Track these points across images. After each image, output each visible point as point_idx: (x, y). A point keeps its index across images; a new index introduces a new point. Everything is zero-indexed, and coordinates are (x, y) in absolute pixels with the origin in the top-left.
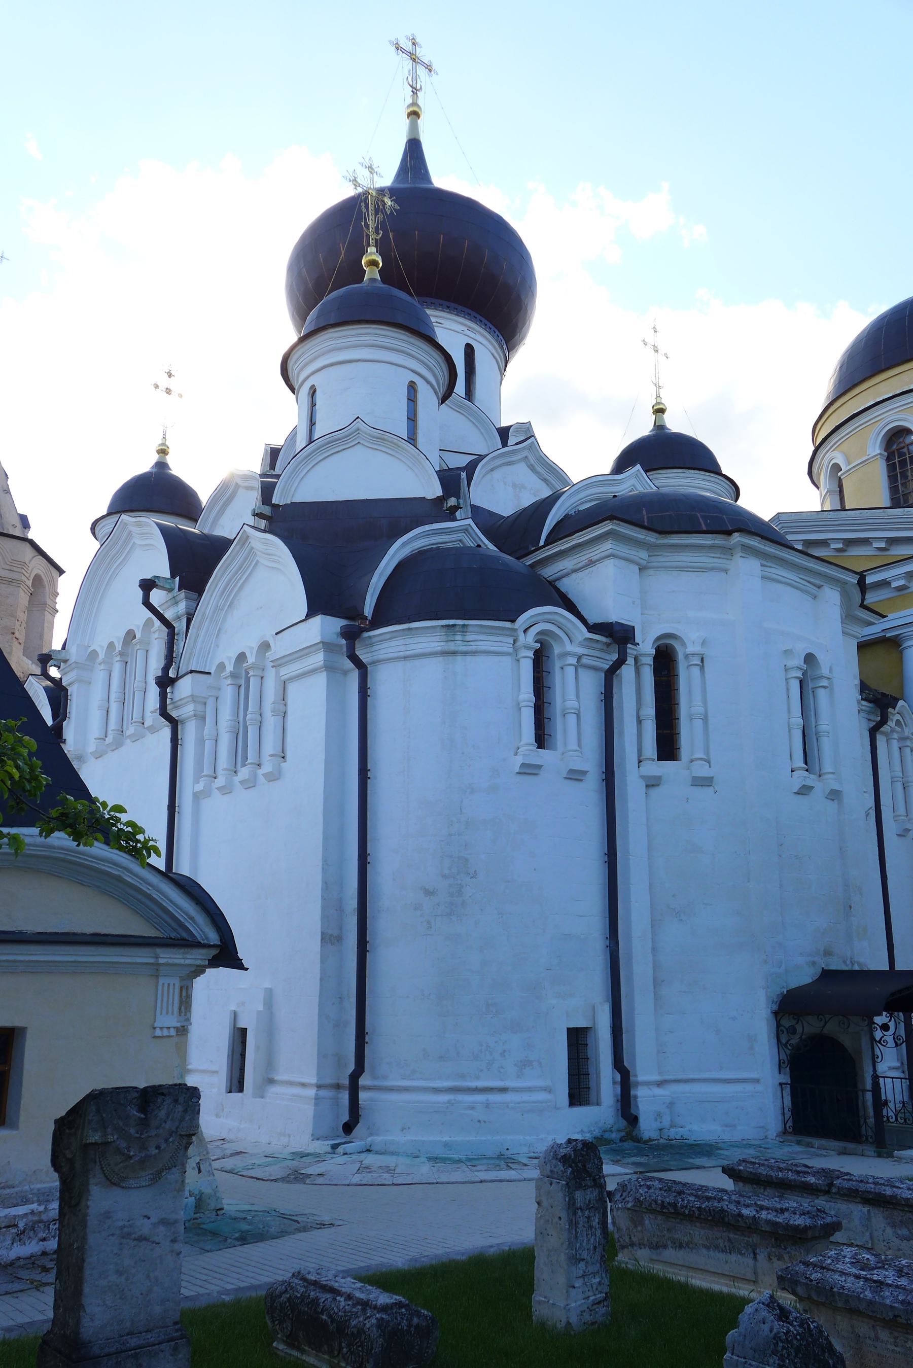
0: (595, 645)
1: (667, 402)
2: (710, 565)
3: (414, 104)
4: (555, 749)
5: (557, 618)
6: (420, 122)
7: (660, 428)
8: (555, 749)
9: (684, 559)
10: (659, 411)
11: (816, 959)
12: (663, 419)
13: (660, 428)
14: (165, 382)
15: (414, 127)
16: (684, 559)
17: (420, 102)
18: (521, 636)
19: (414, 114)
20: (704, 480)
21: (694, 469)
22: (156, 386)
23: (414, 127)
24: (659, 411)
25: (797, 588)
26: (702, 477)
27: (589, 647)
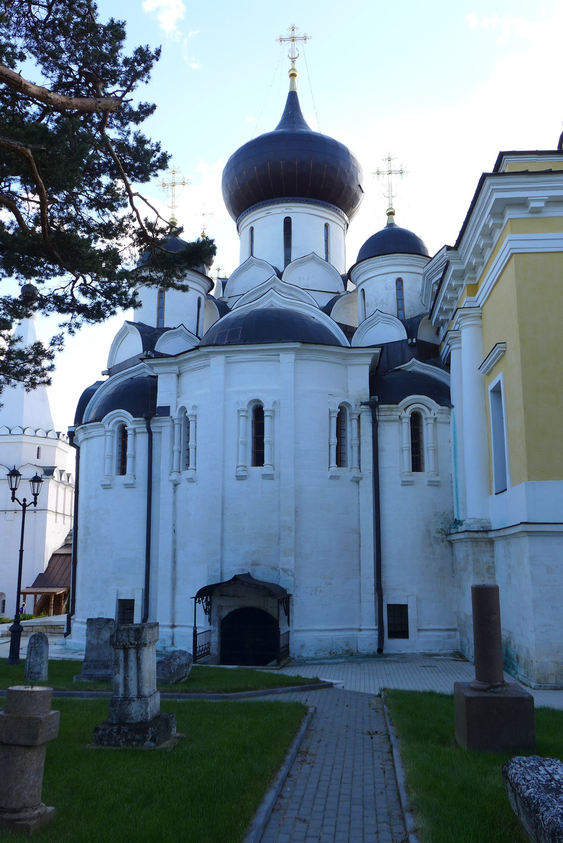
0: (140, 422)
1: (396, 208)
2: (202, 365)
3: (293, 69)
4: (347, 467)
5: (121, 414)
6: (296, 79)
7: (391, 225)
8: (347, 467)
9: (191, 365)
10: (391, 214)
11: (244, 568)
12: (392, 219)
13: (391, 225)
14: (384, 167)
15: (293, 83)
16: (191, 365)
17: (296, 67)
18: (107, 427)
19: (293, 75)
20: (383, 261)
21: (375, 256)
22: (378, 173)
23: (293, 83)
24: (391, 214)
25: (252, 361)
26: (381, 259)
27: (137, 424)
